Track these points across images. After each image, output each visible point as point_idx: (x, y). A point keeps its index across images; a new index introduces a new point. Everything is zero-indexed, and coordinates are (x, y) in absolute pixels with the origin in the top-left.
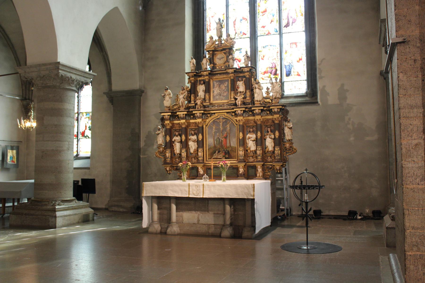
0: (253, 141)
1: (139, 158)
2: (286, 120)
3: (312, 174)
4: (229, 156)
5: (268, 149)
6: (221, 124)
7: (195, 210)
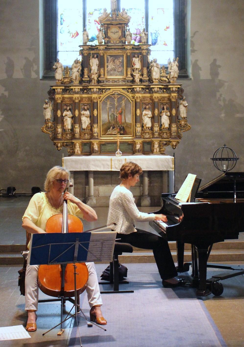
0: (149, 118)
2: (182, 99)
4: (124, 132)
5: (164, 126)
6: (116, 100)
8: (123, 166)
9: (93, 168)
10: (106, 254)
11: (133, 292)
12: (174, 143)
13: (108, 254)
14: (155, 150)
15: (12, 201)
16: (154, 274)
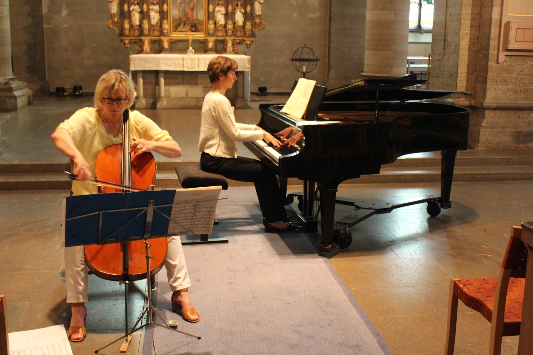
1: (43, 27)
3: (310, 49)
7: (183, 84)
8: (209, 65)
9: (163, 68)
10: (201, 223)
11: (227, 242)
12: (248, 42)
13: (204, 222)
14: (228, 49)
15: (78, 101)
16: (247, 205)
